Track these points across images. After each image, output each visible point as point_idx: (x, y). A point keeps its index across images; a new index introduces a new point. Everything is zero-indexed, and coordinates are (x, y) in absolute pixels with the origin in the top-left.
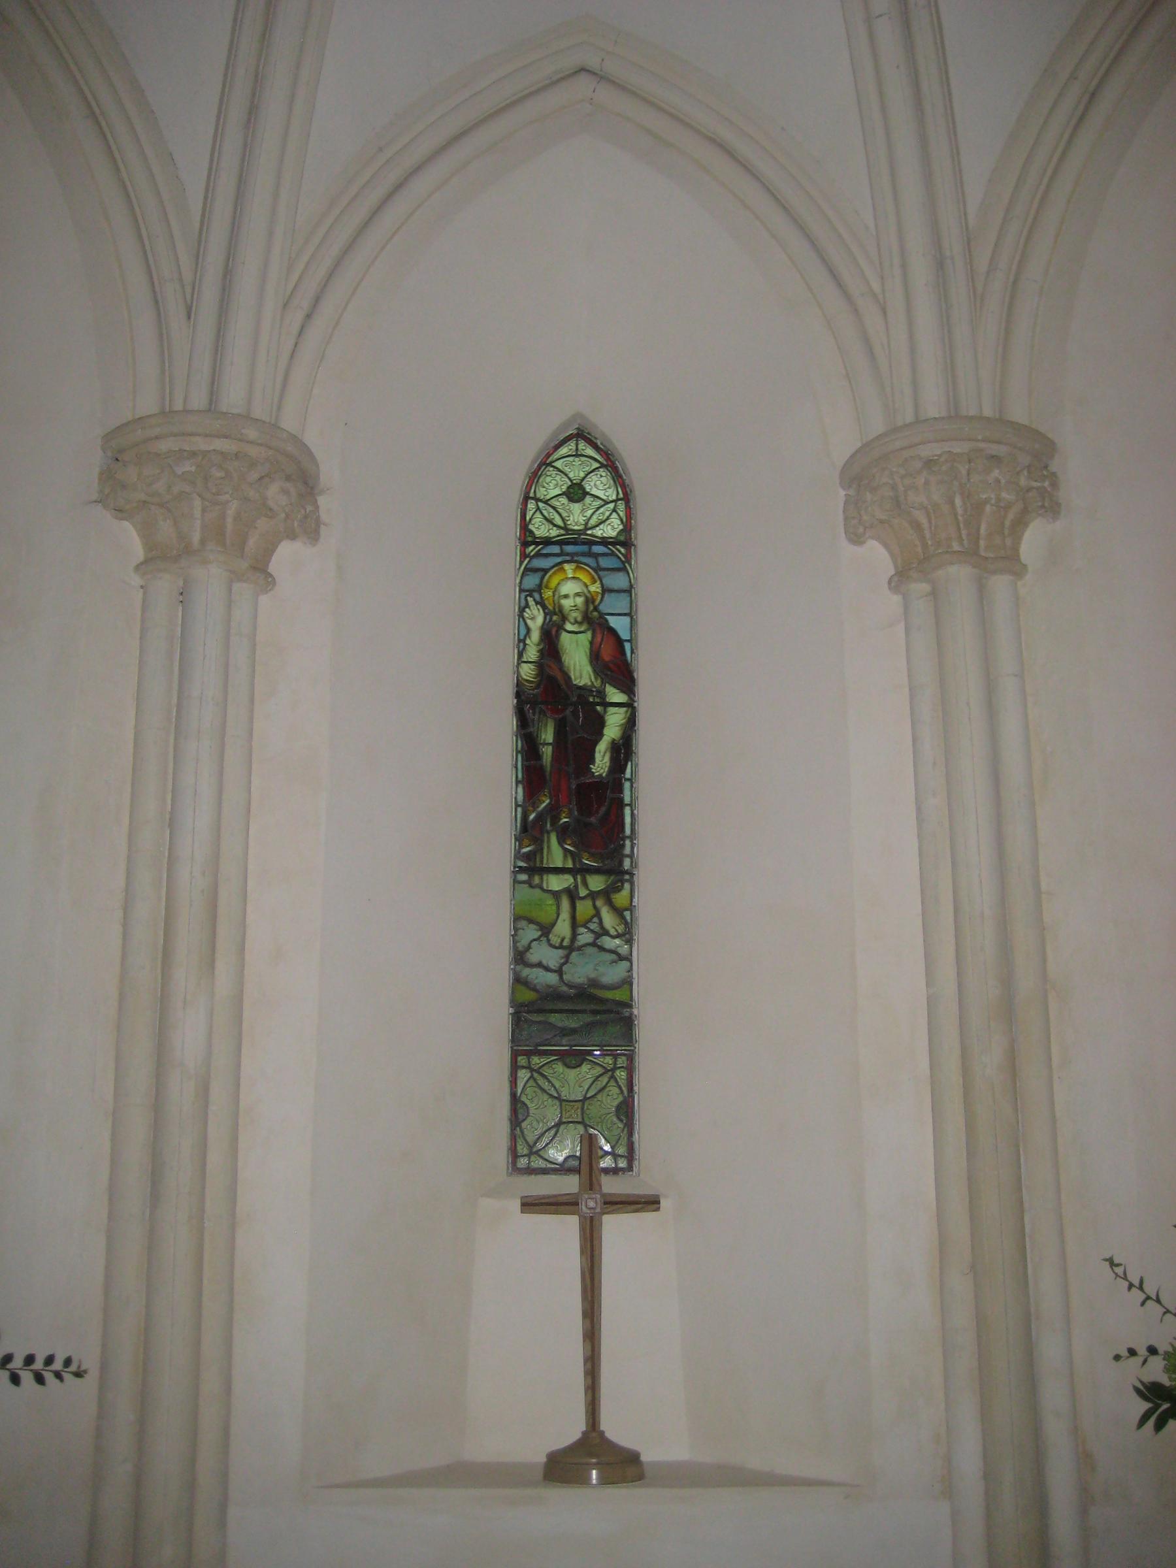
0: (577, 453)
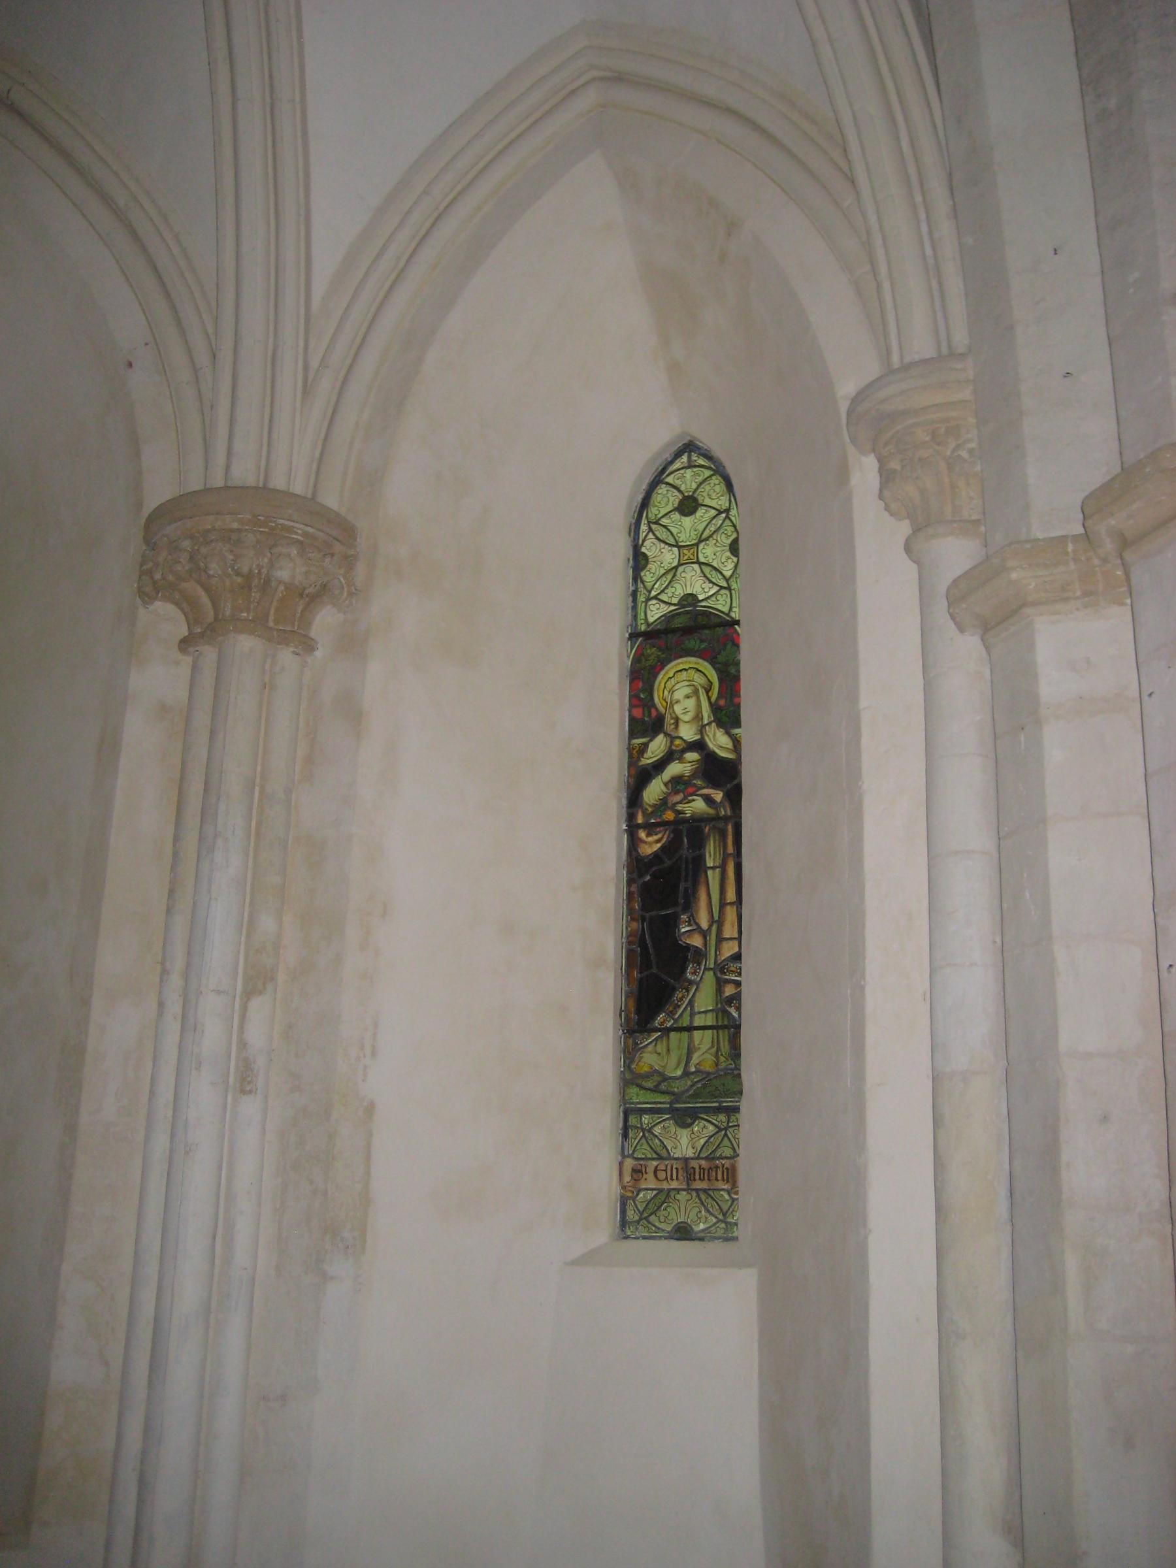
0: (691, 1039)
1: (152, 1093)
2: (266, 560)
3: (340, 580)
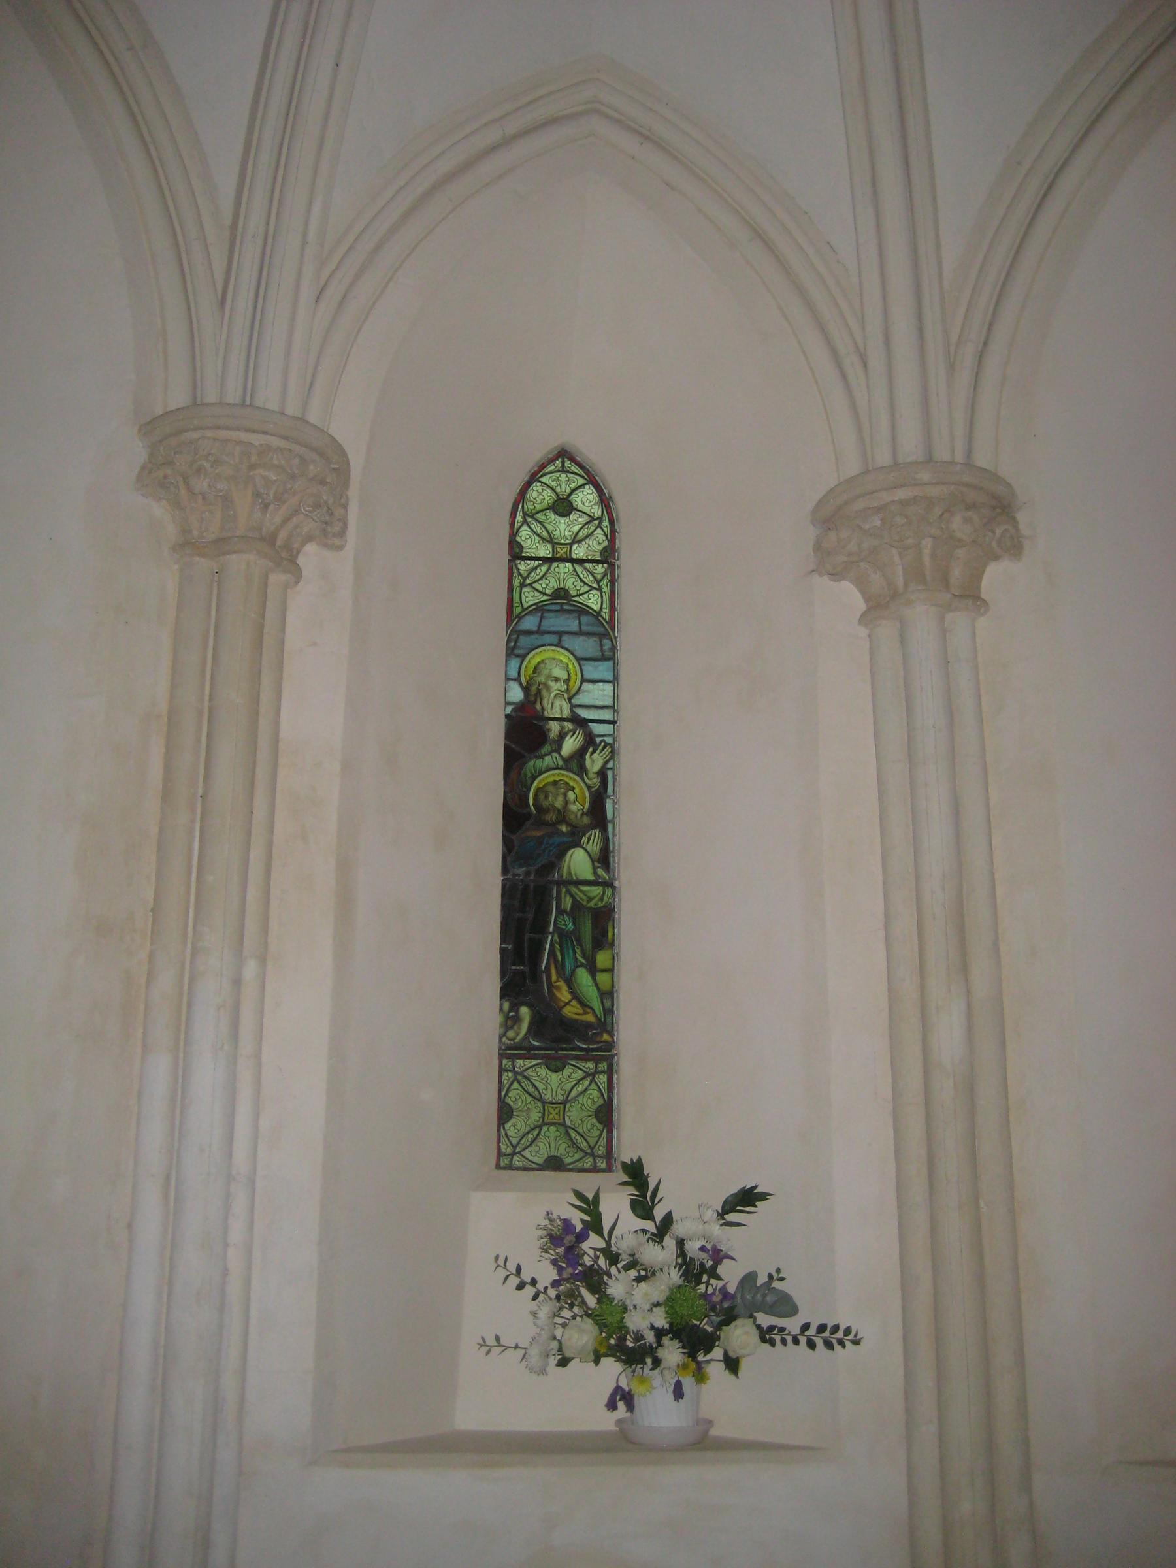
0: (563, 469)
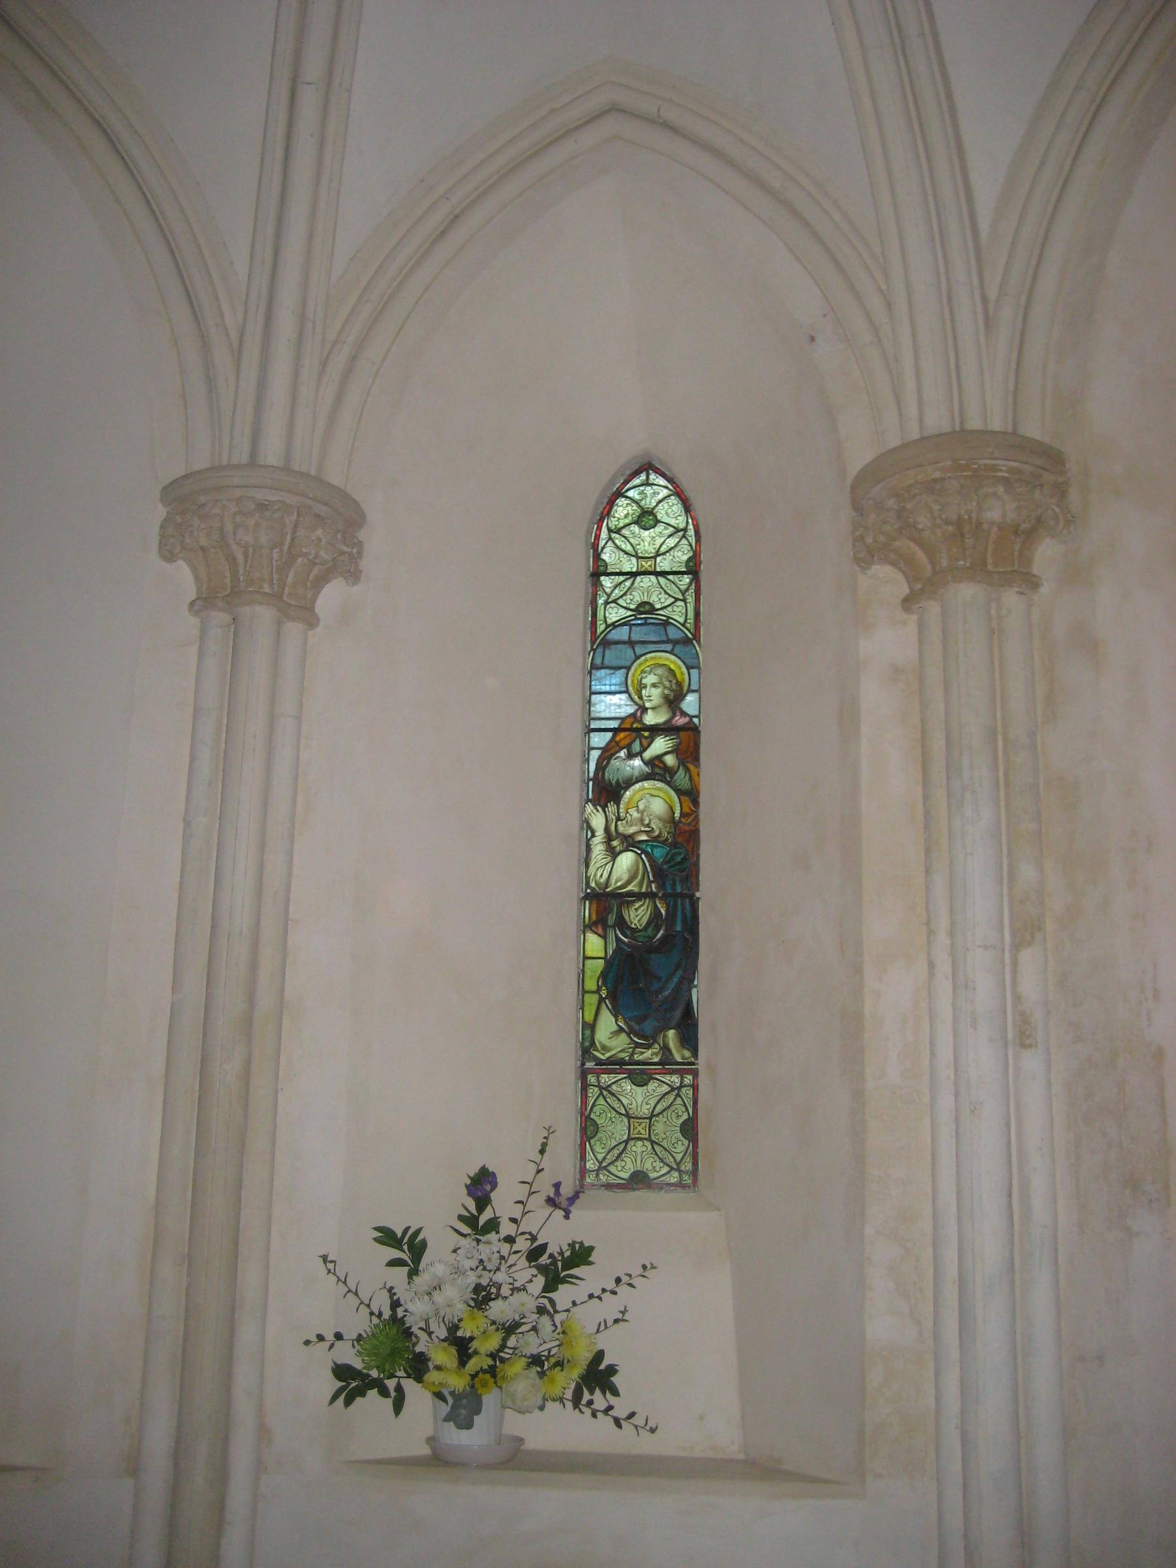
1: (933, 1054)
2: (974, 504)
3: (1053, 510)
